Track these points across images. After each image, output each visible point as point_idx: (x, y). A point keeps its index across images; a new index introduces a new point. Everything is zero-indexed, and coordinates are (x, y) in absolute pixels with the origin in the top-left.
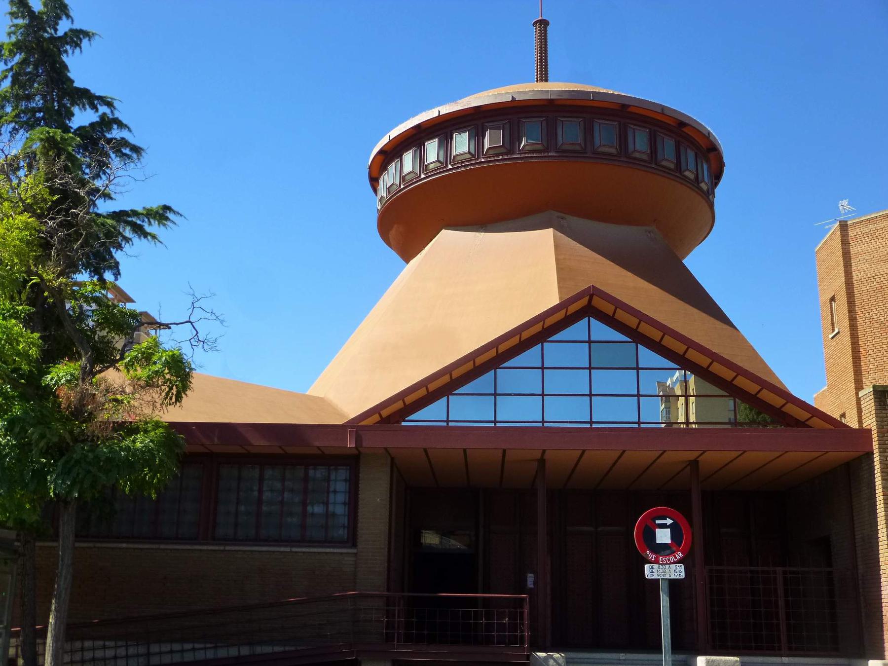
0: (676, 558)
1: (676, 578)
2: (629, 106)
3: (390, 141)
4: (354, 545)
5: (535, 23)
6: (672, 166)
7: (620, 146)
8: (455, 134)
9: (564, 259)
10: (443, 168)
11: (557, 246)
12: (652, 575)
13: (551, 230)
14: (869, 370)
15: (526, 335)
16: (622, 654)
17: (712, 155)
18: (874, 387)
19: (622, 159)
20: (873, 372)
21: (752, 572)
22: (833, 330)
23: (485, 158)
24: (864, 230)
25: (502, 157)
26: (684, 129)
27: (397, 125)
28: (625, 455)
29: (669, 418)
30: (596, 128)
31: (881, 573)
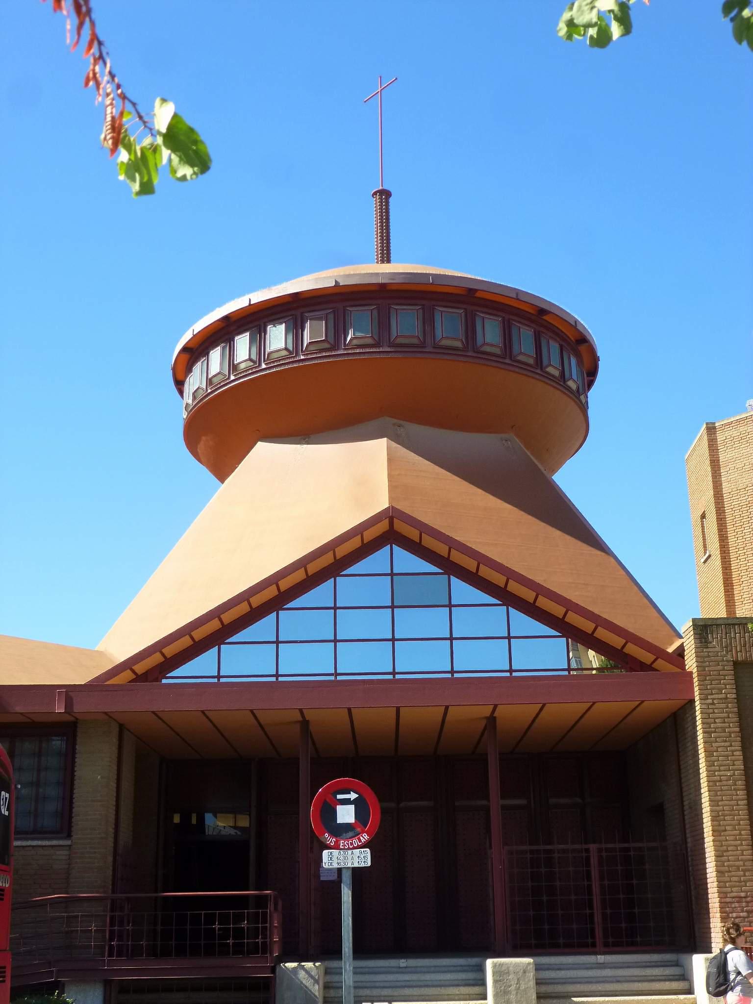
0: (360, 841)
1: (359, 866)
2: (476, 290)
3: (194, 336)
4: (69, 836)
5: (375, 193)
6: (531, 361)
7: (467, 338)
8: (269, 327)
9: (399, 475)
10: (255, 368)
11: (391, 460)
12: (331, 863)
13: (385, 439)
14: (742, 600)
15: (313, 568)
16: (403, 960)
17: (583, 348)
18: (694, 620)
19: (470, 354)
20: (747, 602)
21: (532, 852)
22: (705, 553)
23: (304, 354)
24: (735, 433)
25: (324, 354)
26: (545, 317)
27: (200, 317)
28: (545, 708)
29: (580, 663)
30: (438, 317)
31: (706, 847)
